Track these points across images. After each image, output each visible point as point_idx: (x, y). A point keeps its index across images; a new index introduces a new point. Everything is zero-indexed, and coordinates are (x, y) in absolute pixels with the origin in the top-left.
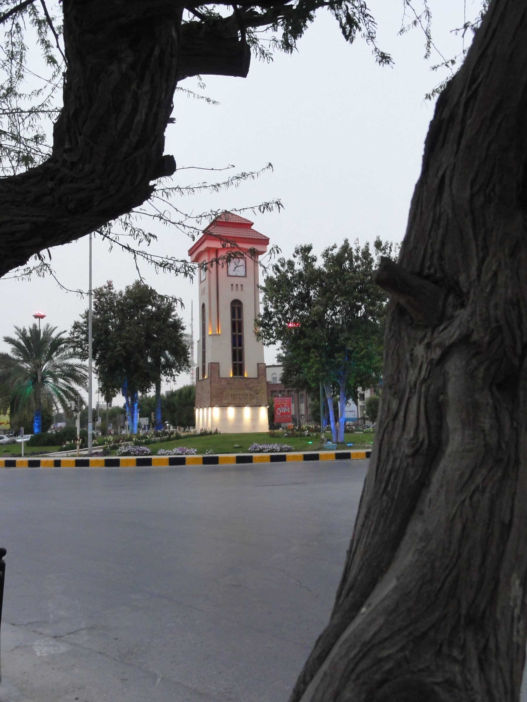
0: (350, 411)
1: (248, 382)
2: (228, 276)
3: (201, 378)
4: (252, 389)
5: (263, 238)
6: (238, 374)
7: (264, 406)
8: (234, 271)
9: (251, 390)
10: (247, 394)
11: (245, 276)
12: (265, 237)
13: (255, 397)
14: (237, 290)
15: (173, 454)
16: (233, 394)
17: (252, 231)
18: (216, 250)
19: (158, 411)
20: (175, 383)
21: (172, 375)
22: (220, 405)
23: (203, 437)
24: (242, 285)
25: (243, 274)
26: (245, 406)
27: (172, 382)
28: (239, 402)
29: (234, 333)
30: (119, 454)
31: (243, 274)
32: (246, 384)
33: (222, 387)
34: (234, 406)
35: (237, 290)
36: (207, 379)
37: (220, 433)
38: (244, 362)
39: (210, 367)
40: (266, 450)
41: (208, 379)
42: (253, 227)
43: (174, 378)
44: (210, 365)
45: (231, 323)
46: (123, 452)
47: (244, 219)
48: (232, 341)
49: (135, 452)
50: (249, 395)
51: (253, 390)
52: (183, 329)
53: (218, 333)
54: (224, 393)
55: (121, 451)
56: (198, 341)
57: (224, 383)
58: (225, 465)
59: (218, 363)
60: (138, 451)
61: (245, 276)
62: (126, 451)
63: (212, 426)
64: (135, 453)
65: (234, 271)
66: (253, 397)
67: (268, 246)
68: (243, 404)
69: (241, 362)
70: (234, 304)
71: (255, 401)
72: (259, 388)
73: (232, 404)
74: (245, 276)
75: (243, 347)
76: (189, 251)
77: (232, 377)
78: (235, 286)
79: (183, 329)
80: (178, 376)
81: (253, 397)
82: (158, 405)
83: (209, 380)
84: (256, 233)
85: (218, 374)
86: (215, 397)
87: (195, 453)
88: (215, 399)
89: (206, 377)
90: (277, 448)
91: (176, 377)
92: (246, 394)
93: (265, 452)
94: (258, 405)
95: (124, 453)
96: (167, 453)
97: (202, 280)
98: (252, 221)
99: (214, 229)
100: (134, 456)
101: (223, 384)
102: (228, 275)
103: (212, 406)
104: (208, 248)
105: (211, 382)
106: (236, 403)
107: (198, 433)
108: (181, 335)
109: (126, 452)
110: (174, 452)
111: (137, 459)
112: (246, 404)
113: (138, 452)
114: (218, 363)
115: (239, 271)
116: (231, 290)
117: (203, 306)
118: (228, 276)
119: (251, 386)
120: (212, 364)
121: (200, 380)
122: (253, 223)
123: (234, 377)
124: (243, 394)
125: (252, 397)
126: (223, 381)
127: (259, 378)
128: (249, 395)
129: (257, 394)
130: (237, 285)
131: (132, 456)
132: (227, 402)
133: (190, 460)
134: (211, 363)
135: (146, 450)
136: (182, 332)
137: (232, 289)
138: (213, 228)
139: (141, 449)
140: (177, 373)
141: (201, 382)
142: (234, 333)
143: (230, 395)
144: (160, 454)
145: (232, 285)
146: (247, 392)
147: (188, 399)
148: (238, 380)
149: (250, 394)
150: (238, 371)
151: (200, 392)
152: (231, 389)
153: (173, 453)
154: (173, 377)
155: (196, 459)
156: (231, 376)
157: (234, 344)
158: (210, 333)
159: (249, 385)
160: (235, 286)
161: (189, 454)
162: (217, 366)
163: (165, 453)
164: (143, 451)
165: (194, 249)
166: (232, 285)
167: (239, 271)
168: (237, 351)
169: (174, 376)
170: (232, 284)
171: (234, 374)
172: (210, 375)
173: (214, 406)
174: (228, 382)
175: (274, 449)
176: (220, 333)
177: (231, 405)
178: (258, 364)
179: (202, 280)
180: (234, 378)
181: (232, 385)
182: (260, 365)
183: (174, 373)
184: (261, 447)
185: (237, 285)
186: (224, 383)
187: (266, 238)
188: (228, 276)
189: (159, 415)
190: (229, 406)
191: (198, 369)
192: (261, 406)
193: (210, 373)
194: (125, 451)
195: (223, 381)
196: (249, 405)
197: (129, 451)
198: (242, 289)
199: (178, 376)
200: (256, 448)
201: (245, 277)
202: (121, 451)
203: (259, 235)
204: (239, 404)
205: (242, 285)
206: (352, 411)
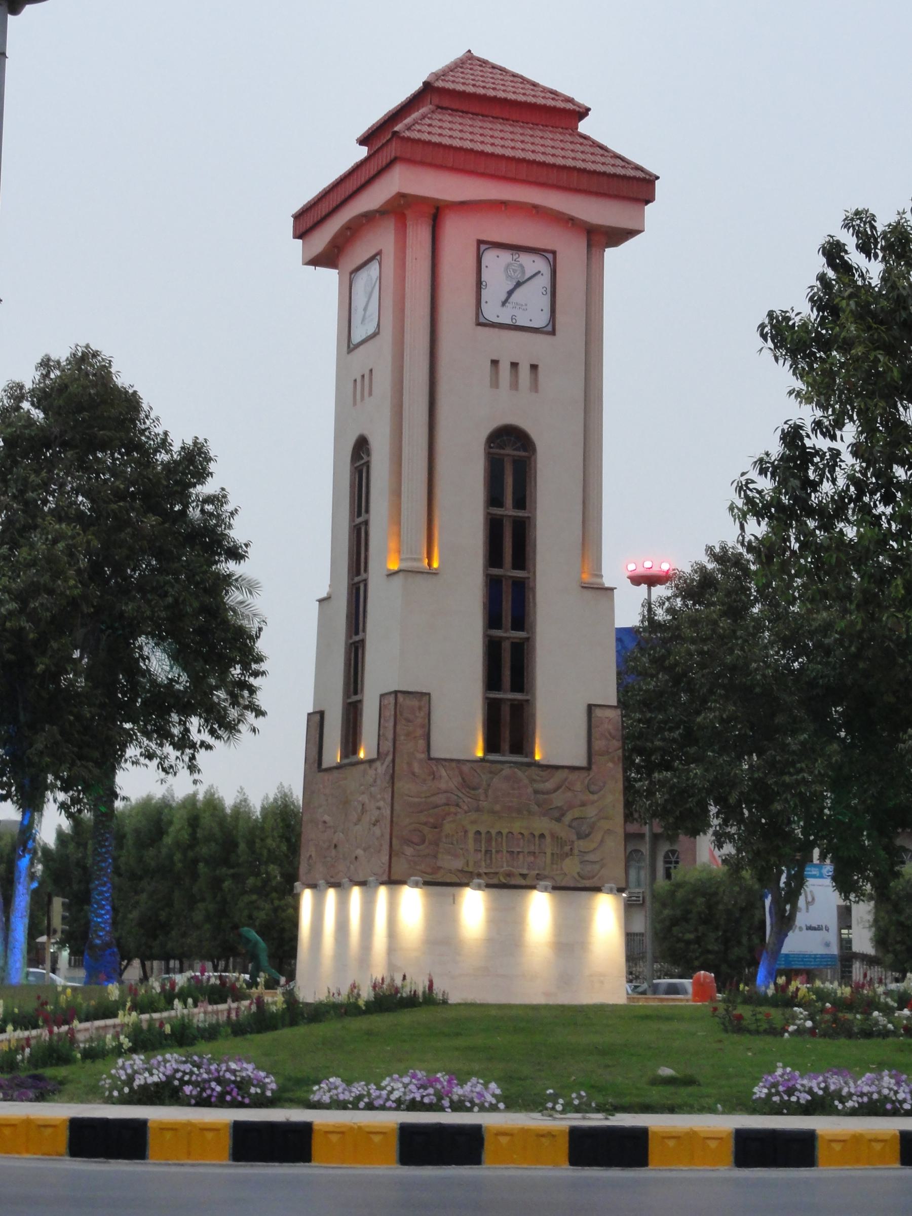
0: (810, 928)
1: (549, 785)
2: (482, 323)
3: (333, 754)
4: (563, 815)
5: (631, 173)
6: (506, 746)
7: (610, 891)
8: (504, 303)
9: (558, 820)
10: (542, 836)
11: (551, 330)
12: (638, 168)
13: (576, 852)
14: (515, 385)
15: (389, 1104)
16: (483, 830)
17: (585, 142)
18: (433, 211)
19: (101, 893)
20: (196, 776)
21: (184, 743)
22: (428, 878)
23: (380, 1021)
24: (534, 367)
25: (540, 320)
26: (533, 887)
27: (184, 773)
28: (506, 868)
29: (496, 571)
30: (120, 1091)
31: (540, 320)
32: (536, 792)
33: (441, 799)
34: (489, 886)
35: (515, 385)
36: (370, 762)
37: (445, 1002)
38: (533, 695)
39: (389, 713)
40: (850, 1104)
41: (378, 764)
42: (584, 127)
43: (193, 758)
44: (391, 699)
45: (486, 523)
46: (139, 1081)
47: (545, 90)
48: (484, 604)
49: (202, 1085)
50: (548, 839)
51: (567, 818)
52: (236, 554)
53: (430, 564)
54: (448, 827)
55: (131, 1079)
56: (321, 601)
57: (447, 780)
58: (684, 1172)
59: (429, 694)
60: (219, 1081)
61: (550, 328)
62: (155, 1079)
63: (391, 966)
64: (203, 1090)
65: (504, 303)
66: (567, 849)
67: (648, 208)
68: (524, 876)
69: (518, 696)
70: (501, 447)
71: (571, 866)
72: (591, 812)
73: (479, 875)
74: (551, 330)
75: (532, 630)
76: (298, 217)
77: (482, 760)
78: (505, 368)
79: (236, 554)
80: (209, 747)
81: (567, 849)
82: (101, 869)
83: (381, 768)
84: (602, 152)
85: (422, 743)
86: (409, 842)
87: (501, 1106)
88: (409, 851)
89: (362, 755)
90: (901, 1096)
91: (202, 756)
92: (537, 833)
93: (838, 1113)
94: (588, 883)
95: (145, 1087)
96: (359, 1098)
97: (357, 337)
98: (582, 99)
99: (427, 121)
100: (197, 1104)
101: (443, 786)
102: (482, 320)
103: (393, 882)
104: (401, 196)
105: (392, 777)
106: (496, 873)
107: (404, 995)
108: (227, 580)
109: (156, 1084)
110: (395, 1095)
111: (239, 1128)
112: (539, 877)
113: (218, 1089)
114: (429, 694)
115: (523, 307)
116: (491, 386)
117: (361, 447)
118: (479, 324)
119: (559, 800)
120: (401, 698)
121: (325, 765)
122: (588, 110)
123: (492, 757)
124: (526, 833)
125: (564, 851)
126: (443, 773)
127: (594, 767)
128: (548, 839)
129: (581, 836)
130: (514, 365)
131: (189, 1105)
132: (458, 864)
133: (504, 1140)
134: (396, 693)
135: (259, 1081)
136: (231, 567)
137: (495, 383)
138: (424, 117)
139: (234, 1072)
140: (206, 737)
141: (336, 774)
142: (496, 571)
143: (471, 835)
144: (326, 1099)
145: (495, 363)
146: (542, 824)
147: (152, 852)
148: (507, 771)
149: (554, 836)
150: (506, 734)
151: (326, 818)
152: (478, 810)
153: (388, 1099)
154: (188, 751)
155: (542, 1135)
156: (480, 754)
157: (493, 619)
158: (393, 566)
159: (554, 795)
160: (505, 368)
161: (470, 1110)
162: (420, 708)
163: (347, 1096)
164: (243, 1085)
165: (324, 208)
166: (495, 363)
167: (523, 307)
168: (506, 646)
169: (193, 746)
170: (495, 358)
171: (491, 746)
172: (388, 745)
173: (403, 882)
174: (464, 781)
175: (886, 1099)
176: (435, 565)
177: (476, 881)
178: (590, 708)
179: (357, 337)
180: (488, 761)
181: (480, 791)
182: (598, 713)
183: (195, 737)
184: (816, 1084)
185: (514, 365)
186: (447, 780)
187: (642, 175)
188: (482, 323)
189: (102, 907)
190: (467, 885)
191: (318, 717)
192: (598, 889)
193: (390, 735)
194: (150, 1080)
195: (443, 773)
196: (548, 883)
197: (170, 1079)
198: (535, 386)
199: (209, 747)
200: (790, 1091)
201: (548, 333)
202: (131, 1079)
203: (612, 161)
204: (509, 875)
205: (534, 367)
206: (818, 928)
